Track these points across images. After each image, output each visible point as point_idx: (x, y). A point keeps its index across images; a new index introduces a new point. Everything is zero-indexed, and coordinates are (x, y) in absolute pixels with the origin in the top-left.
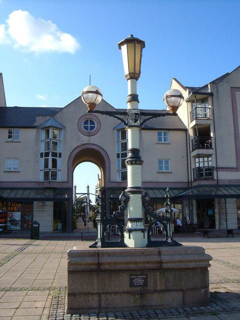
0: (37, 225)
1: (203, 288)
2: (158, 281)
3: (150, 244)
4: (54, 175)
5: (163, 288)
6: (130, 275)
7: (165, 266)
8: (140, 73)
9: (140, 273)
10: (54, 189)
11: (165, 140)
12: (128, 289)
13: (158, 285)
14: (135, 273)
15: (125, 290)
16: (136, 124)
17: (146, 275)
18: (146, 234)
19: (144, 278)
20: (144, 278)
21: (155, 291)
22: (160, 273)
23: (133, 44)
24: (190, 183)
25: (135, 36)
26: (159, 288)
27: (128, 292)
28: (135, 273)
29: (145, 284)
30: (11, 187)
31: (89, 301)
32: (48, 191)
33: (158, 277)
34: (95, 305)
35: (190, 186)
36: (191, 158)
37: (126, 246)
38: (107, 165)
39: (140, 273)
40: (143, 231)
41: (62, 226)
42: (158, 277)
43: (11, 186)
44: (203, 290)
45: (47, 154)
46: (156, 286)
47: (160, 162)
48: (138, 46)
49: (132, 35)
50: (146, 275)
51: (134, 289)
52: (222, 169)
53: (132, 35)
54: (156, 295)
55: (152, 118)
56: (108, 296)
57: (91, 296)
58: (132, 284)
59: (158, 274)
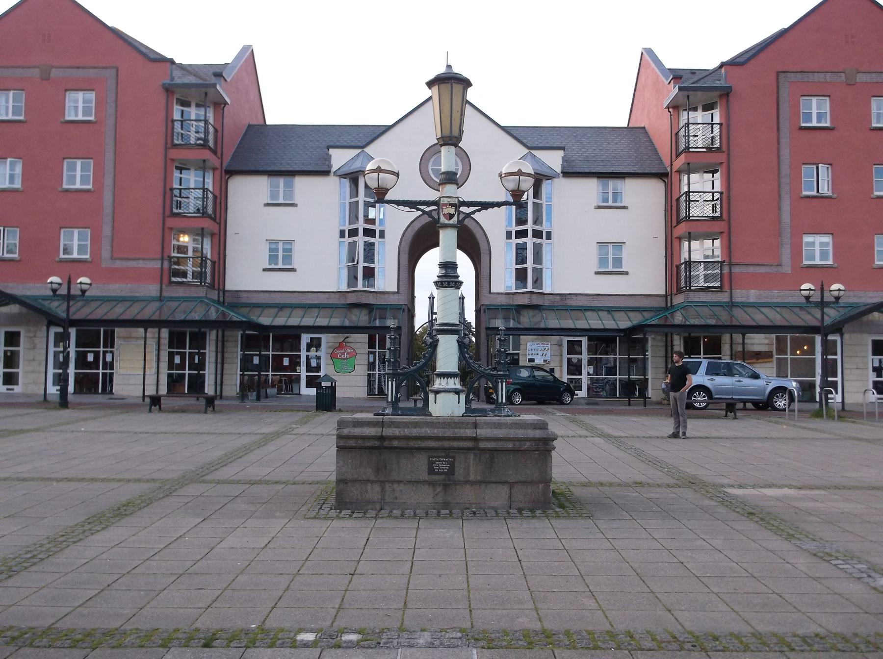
0: (329, 384)
1: (540, 482)
2: (471, 468)
3: (469, 410)
4: (369, 273)
5: (479, 478)
6: (429, 457)
7: (482, 445)
8: (461, 132)
9: (443, 454)
10: (369, 307)
11: (615, 201)
12: (426, 477)
13: (471, 474)
14: (436, 454)
15: (421, 477)
16: (451, 222)
17: (453, 457)
18: (463, 397)
19: (449, 463)
20: (449, 463)
21: (467, 482)
22: (475, 455)
23: (449, 85)
24: (669, 298)
25: (456, 70)
26: (472, 477)
27: (424, 482)
28: (436, 454)
29: (452, 470)
30: (277, 302)
31: (367, 492)
32: (356, 311)
33: (472, 462)
34: (376, 498)
35: (669, 305)
36: (674, 240)
37: (430, 415)
38: (484, 258)
39: (443, 454)
40: (457, 392)
41: (86, 357)
42: (472, 462)
43: (278, 299)
44: (541, 486)
45: (353, 233)
46: (468, 475)
47: (602, 245)
48: (458, 88)
49: (449, 67)
50: (453, 457)
51: (435, 477)
52: (679, 281)
53: (449, 67)
54: (468, 488)
55: (479, 210)
56: (395, 486)
57: (370, 484)
58: (431, 471)
59: (472, 456)
